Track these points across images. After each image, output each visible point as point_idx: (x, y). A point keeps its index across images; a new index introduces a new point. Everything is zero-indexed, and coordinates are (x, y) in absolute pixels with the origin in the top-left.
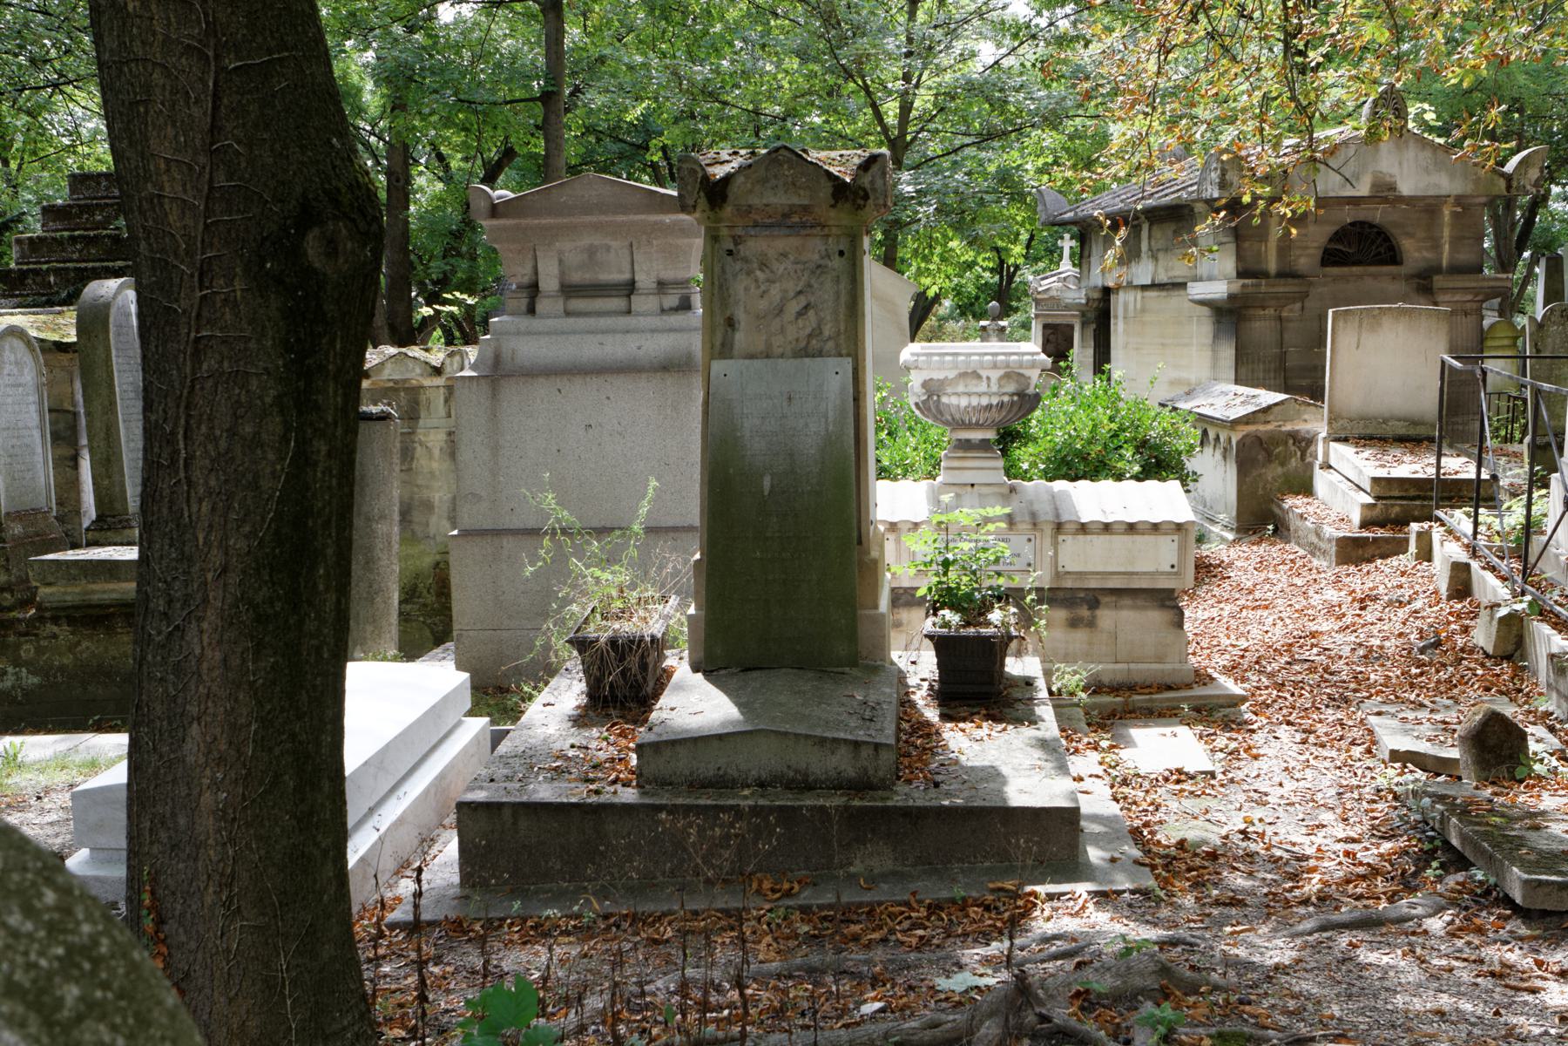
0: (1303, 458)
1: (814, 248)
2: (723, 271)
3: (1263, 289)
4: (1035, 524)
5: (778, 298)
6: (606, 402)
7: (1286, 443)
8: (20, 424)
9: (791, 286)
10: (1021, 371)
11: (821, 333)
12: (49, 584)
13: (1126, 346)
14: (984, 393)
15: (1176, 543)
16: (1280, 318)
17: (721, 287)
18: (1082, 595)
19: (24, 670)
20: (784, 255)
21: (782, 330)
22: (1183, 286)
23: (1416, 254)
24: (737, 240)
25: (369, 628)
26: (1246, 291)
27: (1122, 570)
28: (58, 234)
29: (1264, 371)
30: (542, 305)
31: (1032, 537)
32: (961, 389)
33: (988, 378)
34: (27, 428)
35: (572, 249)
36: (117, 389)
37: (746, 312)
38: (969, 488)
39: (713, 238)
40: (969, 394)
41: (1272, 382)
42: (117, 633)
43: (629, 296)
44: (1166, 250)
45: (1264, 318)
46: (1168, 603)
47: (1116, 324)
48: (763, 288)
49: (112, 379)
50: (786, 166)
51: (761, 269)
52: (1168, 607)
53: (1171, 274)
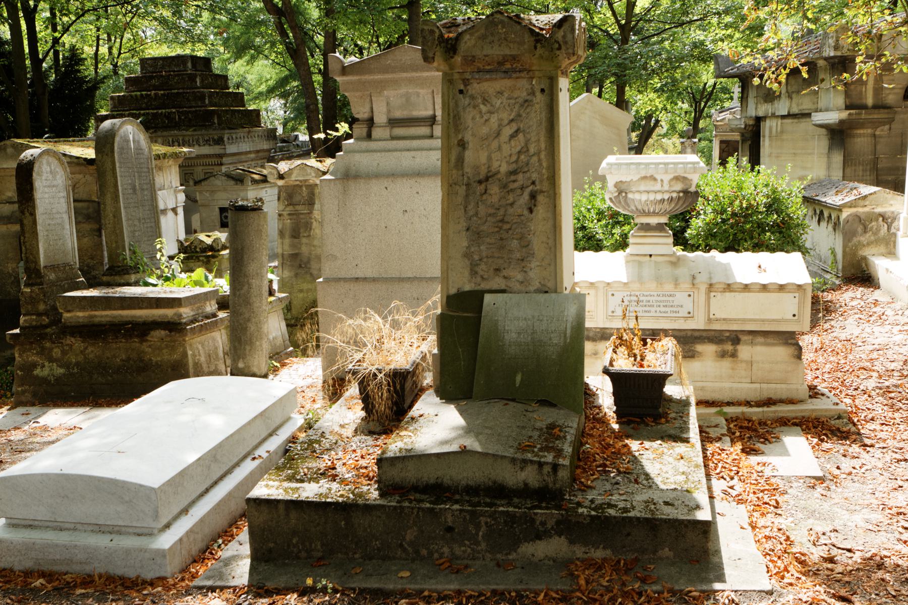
0: (889, 228)
1: (522, 87)
2: (457, 105)
3: (863, 116)
4: (693, 285)
5: (496, 125)
6: (416, 195)
7: (877, 220)
8: (54, 211)
9: (506, 116)
10: (686, 175)
11: (528, 150)
12: (69, 311)
13: (770, 155)
14: (659, 191)
15: (797, 298)
16: (874, 136)
17: (454, 117)
18: (727, 334)
19: (55, 364)
20: (500, 93)
21: (500, 148)
22: (808, 115)
24: (466, 82)
25: (248, 348)
26: (851, 118)
27: (757, 317)
28: (133, 94)
29: (863, 170)
30: (376, 133)
31: (692, 294)
32: (642, 188)
33: (662, 181)
34: (58, 213)
35: (394, 95)
36: (120, 188)
37: (473, 135)
38: (648, 257)
39: (448, 80)
40: (648, 192)
41: (868, 178)
42: (110, 343)
43: (432, 126)
45: (863, 135)
46: (790, 341)
47: (764, 141)
48: (485, 117)
49: (117, 182)
50: (500, 27)
51: (483, 104)
52: (791, 344)
53: (801, 108)
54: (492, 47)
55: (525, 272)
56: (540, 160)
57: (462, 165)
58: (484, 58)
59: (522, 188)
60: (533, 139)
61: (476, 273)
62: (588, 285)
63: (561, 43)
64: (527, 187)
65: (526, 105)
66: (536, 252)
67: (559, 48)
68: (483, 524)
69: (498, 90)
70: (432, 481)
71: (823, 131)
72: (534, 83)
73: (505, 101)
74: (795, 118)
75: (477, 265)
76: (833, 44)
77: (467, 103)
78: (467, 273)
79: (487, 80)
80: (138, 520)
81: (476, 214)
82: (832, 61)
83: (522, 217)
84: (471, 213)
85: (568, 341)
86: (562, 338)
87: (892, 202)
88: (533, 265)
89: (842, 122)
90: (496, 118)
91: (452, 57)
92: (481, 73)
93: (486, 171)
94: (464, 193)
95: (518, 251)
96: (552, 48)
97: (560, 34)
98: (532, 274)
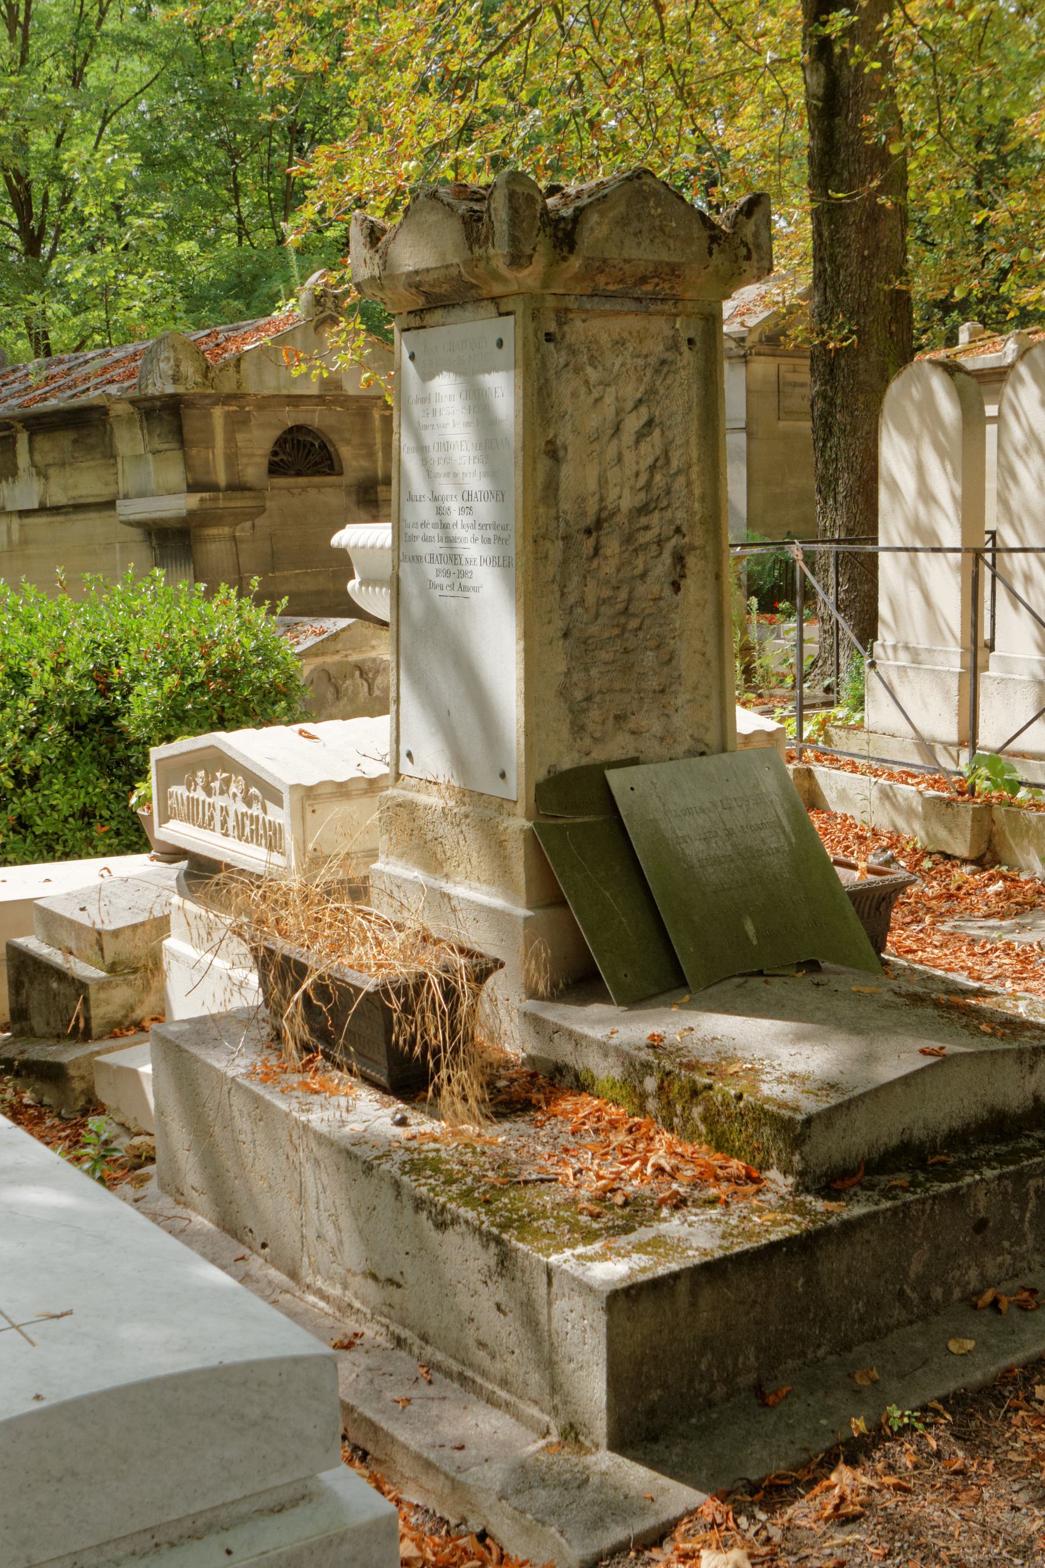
3: (221, 504)
9: (631, 391)
16: (234, 538)
20: (620, 343)
21: (620, 459)
22: (109, 505)
23: (354, 463)
24: (562, 315)
37: (576, 432)
44: (63, 465)
48: (595, 394)
54: (639, 244)
55: (668, 716)
56: (689, 484)
57: (556, 496)
58: (622, 265)
59: (660, 542)
60: (679, 441)
61: (582, 728)
62: (364, 785)
63: (751, 246)
64: (669, 539)
65: (665, 370)
66: (684, 673)
67: (748, 257)
68: (1032, 1194)
69: (616, 337)
70: (895, 1141)
71: (136, 534)
72: (678, 326)
73: (629, 361)
74: (58, 514)
75: (584, 711)
76: (171, 372)
77: (562, 362)
78: (565, 729)
79: (604, 314)
80: (284, 1465)
81: (582, 601)
82: (147, 404)
83: (662, 603)
84: (572, 599)
85: (793, 840)
86: (782, 836)
87: (374, 642)
88: (679, 702)
89: (191, 513)
90: (613, 396)
91: (565, 259)
92: (596, 299)
93: (596, 507)
94: (559, 556)
95: (655, 674)
96: (736, 256)
97: (749, 229)
98: (677, 720)
